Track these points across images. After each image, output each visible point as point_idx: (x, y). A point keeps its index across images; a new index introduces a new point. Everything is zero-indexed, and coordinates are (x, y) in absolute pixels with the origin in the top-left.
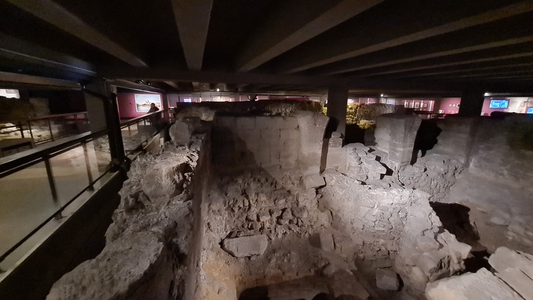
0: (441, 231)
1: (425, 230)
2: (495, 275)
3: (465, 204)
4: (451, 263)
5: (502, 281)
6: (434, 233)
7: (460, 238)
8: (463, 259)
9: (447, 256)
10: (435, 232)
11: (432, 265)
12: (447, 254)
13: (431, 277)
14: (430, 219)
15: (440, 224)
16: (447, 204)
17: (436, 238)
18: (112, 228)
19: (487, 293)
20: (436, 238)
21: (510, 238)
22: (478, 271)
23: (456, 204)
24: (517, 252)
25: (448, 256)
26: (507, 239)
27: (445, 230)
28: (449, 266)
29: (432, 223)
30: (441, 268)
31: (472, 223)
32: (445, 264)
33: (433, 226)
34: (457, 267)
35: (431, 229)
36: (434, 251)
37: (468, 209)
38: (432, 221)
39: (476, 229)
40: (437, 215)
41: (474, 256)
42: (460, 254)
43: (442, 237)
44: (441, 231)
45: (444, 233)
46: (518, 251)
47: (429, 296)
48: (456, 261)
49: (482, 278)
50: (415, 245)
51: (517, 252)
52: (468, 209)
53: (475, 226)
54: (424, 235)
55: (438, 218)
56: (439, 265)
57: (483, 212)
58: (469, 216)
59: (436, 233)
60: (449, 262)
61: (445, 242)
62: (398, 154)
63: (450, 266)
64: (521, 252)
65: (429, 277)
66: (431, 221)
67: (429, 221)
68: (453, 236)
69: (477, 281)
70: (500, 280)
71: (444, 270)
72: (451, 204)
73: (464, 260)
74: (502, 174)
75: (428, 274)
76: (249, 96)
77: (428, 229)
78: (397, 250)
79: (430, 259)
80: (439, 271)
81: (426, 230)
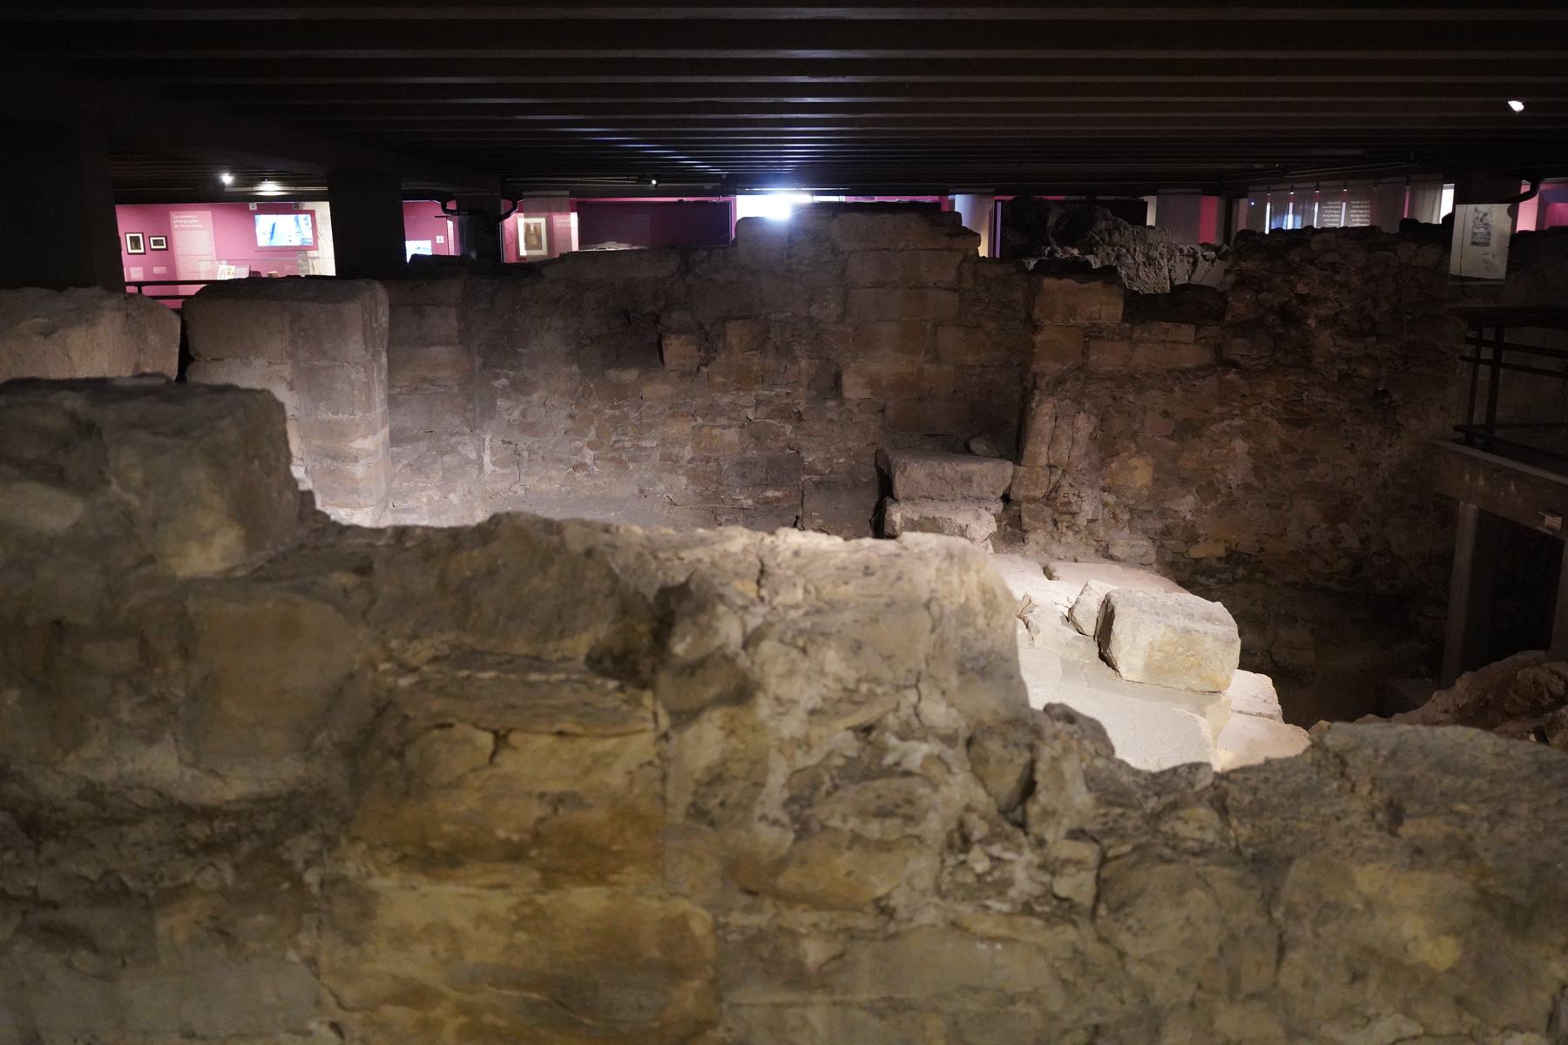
62: (359, 470)
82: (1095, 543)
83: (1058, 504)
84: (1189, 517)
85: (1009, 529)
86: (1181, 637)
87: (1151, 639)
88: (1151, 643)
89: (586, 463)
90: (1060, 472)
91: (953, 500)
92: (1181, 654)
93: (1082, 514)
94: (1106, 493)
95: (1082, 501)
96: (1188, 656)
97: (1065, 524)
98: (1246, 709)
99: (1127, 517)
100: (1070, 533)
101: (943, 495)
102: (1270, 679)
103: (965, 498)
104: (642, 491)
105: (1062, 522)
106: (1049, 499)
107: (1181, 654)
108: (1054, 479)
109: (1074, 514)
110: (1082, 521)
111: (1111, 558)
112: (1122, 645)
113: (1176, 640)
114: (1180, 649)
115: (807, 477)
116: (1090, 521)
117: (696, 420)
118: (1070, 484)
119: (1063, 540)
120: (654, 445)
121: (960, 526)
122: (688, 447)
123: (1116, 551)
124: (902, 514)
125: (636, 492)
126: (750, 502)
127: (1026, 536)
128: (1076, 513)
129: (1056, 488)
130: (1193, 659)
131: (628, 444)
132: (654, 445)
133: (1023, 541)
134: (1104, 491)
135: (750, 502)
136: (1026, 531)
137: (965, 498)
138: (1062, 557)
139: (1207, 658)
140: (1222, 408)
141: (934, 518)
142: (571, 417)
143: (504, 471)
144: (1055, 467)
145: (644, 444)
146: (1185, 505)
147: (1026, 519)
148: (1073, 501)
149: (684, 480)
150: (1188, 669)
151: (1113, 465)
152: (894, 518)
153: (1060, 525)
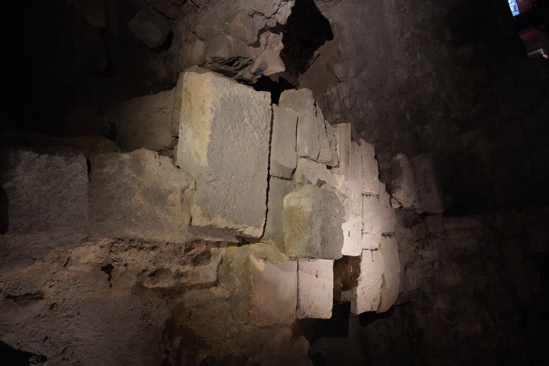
0: (276, 29)
1: (259, 13)
2: (271, 105)
3: (335, 30)
4: (247, 68)
5: (271, 114)
6: (266, 25)
7: (285, 55)
8: (263, 73)
9: (250, 58)
10: (268, 25)
11: (223, 53)
12: (254, 57)
13: (209, 65)
14: (280, 5)
15: (284, 21)
16: (320, 13)
17: (261, 31)
18: (198, 246)
19: (245, 113)
20: (261, 31)
21: (328, 93)
22: (259, 92)
23: (328, 20)
24: (315, 103)
25: (251, 60)
26: (325, 91)
27: (281, 34)
28: (240, 70)
29: (276, 12)
30: (231, 64)
31: (316, 53)
32: (238, 64)
33: (272, 16)
34: (248, 76)
35: (268, 18)
36: (243, 43)
37: (330, 37)
38: (279, 11)
39: (313, 61)
40: (293, 9)
41: (278, 82)
42: (267, 67)
43: (268, 37)
44: (276, 29)
45: (277, 35)
46: (317, 103)
47: (183, 77)
48: (253, 70)
49: (257, 99)
50: (230, 18)
51: (315, 103)
52: (330, 37)
53: (314, 59)
54: (252, 16)
55: (289, 13)
56: (231, 60)
57: (339, 52)
58: (323, 44)
59: (268, 27)
60: (246, 66)
61: (266, 45)
63: (243, 70)
64: (318, 106)
65: (207, 63)
66: (278, 9)
67: (276, 7)
68: (281, 45)
69: (248, 98)
70: (271, 112)
71: (232, 68)
72: (323, 16)
73: (263, 76)
74: (402, 34)
75: (209, 60)
76: (528, 55)
77: (263, 15)
78: (200, 7)
79: (229, 46)
80: (226, 65)
81: (261, 13)
82: (411, 261)
83: (427, 240)
84: (435, 307)
85: (411, 220)
86: (307, 222)
87: (304, 207)
88: (302, 206)
89: (404, 35)
90: (444, 237)
91: (416, 186)
92: (299, 225)
93: (424, 252)
94: (439, 264)
95: (431, 250)
96: (299, 228)
97: (418, 245)
98: (301, 293)
99: (429, 276)
100: (414, 249)
101: (417, 180)
102: (329, 318)
103: (419, 192)
104: (397, 62)
105: (419, 244)
106: (429, 235)
107: (299, 225)
108: (439, 235)
109: (423, 248)
110: (421, 252)
111: (405, 269)
112: (299, 192)
113: (306, 219)
114: (302, 223)
115: (419, 129)
116: (421, 256)
117: (434, 73)
118: (438, 243)
119: (409, 245)
120: (419, 60)
121: (400, 186)
122: (421, 73)
123: (409, 271)
124: (401, 159)
125: (396, 60)
126: (402, 108)
127: (408, 228)
128: (424, 249)
129: (436, 237)
130: (298, 231)
131: (416, 48)
132: (419, 60)
133: (405, 227)
134: (440, 263)
135: (402, 108)
136: (411, 228)
137: (419, 192)
138: (401, 245)
139: (299, 239)
140: (409, 118)
141: (402, 173)
142: (423, 20)
143: (393, 4)
144: (446, 234)
145: (418, 55)
146: (441, 304)
147: (416, 227)
148: (430, 246)
149: (406, 77)
150: (293, 231)
151: (454, 265)
152: (398, 155)
153: (417, 243)
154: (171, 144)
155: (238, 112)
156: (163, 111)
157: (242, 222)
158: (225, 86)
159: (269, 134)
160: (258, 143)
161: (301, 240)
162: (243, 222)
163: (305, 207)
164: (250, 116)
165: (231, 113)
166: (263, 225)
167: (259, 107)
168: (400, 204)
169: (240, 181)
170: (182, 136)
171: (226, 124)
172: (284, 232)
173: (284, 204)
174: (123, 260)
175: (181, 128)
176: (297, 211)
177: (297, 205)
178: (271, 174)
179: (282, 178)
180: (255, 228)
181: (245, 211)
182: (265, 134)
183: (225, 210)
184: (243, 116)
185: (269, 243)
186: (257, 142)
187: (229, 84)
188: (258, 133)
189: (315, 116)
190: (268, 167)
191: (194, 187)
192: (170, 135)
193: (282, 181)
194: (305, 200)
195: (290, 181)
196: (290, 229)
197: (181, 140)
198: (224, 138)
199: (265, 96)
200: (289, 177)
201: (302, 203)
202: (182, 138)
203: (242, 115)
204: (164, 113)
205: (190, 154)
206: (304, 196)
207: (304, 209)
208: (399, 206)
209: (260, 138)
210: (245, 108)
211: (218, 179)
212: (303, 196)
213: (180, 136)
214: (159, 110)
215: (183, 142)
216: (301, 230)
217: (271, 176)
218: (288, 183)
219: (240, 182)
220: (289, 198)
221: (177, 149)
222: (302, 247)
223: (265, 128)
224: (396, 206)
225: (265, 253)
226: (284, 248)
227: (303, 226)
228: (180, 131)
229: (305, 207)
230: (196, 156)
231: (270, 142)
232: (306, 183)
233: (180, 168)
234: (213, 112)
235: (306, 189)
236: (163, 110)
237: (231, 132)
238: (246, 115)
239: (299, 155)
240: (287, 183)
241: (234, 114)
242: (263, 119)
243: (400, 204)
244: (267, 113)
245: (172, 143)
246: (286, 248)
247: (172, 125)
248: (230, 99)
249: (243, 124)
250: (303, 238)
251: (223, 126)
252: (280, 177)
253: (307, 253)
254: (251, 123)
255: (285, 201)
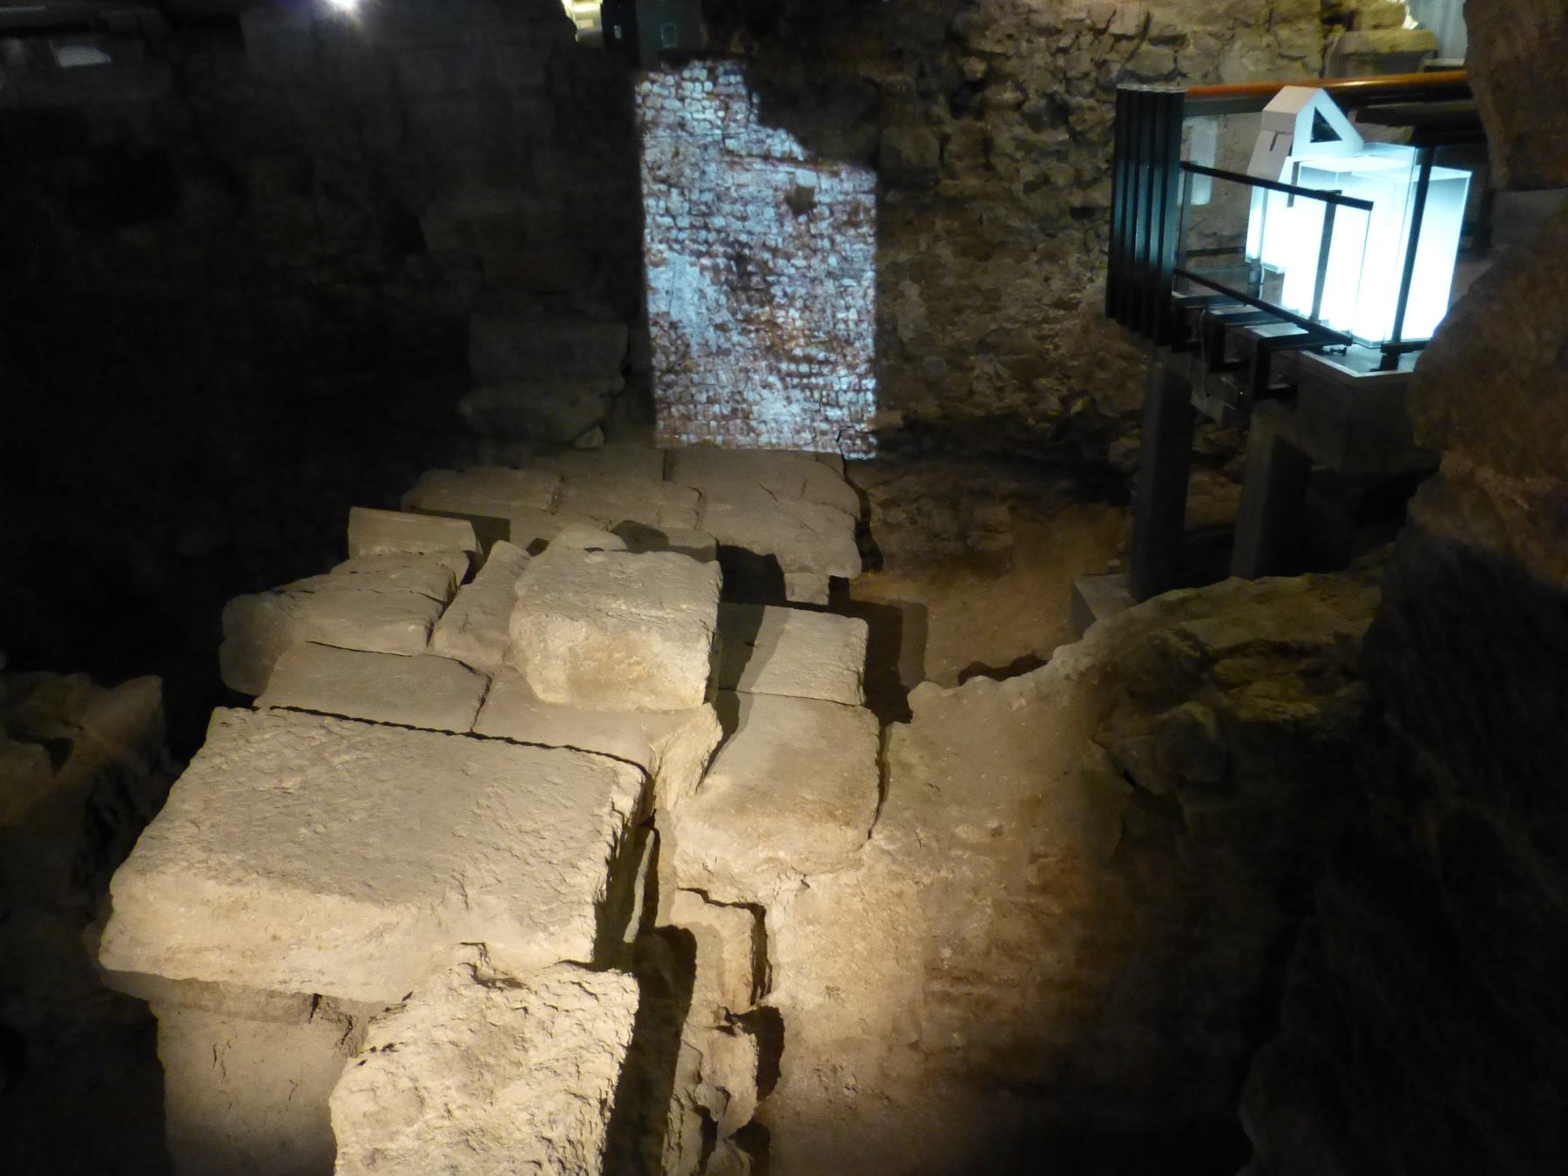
19: (266, 784)
86: (614, 640)
87: (571, 644)
96: (629, 665)
107: (620, 662)
114: (617, 656)
154: (334, 1025)
155: (261, 805)
156: (221, 1048)
157: (597, 818)
158: (167, 838)
159: (346, 724)
160: (367, 755)
161: (662, 662)
162: (597, 815)
163: (573, 641)
164: (281, 771)
165: (261, 826)
166: (610, 763)
167: (256, 742)
168: (591, 427)
169: (474, 813)
170: (310, 981)
171: (294, 842)
172: (635, 707)
173: (560, 702)
174: (553, 937)
175: (284, 985)
176: (582, 665)
177: (565, 664)
178: (468, 730)
179: (483, 701)
180: (618, 784)
181: (566, 807)
182: (345, 733)
183: (555, 861)
184: (277, 792)
185: (663, 753)
186: (365, 758)
187: (166, 825)
188: (337, 753)
189: (312, 596)
190: (445, 735)
191: (475, 947)
192: (306, 1026)
193: (490, 702)
194: (552, 641)
195: (493, 682)
196: (630, 689)
197: (325, 985)
198: (335, 852)
199: (224, 723)
200: (483, 683)
201: (562, 649)
202: (319, 982)
203: (271, 794)
204: (230, 1047)
205: (371, 957)
206: (541, 642)
207: (576, 645)
208: (598, 431)
209: (352, 747)
210: (305, 875)
211: (459, 877)
212: (542, 645)
213: (309, 990)
214: (218, 1065)
215: (330, 979)
216: (634, 658)
217: (471, 730)
218: (498, 686)
219: (478, 816)
220: (542, 686)
221: (351, 1000)
222: (681, 660)
223: (323, 731)
224: (597, 437)
225: (688, 766)
226: (678, 712)
227: (624, 653)
228: (294, 987)
229: (573, 641)
230: (381, 938)
231: (371, 722)
232: (504, 638)
233: (411, 993)
234: (245, 877)
235: (522, 632)
236: (219, 1048)
237: (320, 829)
238: (275, 781)
239: (422, 650)
240: (498, 689)
241: (266, 818)
242: (294, 733)
243: (591, 427)
244: (281, 722)
245: (330, 1020)
246: (680, 707)
247: (275, 1019)
248: (213, 826)
249: (302, 792)
250: (657, 656)
251: (299, 851)
252: (478, 705)
253: (699, 647)
254: (302, 769)
255: (550, 697)
